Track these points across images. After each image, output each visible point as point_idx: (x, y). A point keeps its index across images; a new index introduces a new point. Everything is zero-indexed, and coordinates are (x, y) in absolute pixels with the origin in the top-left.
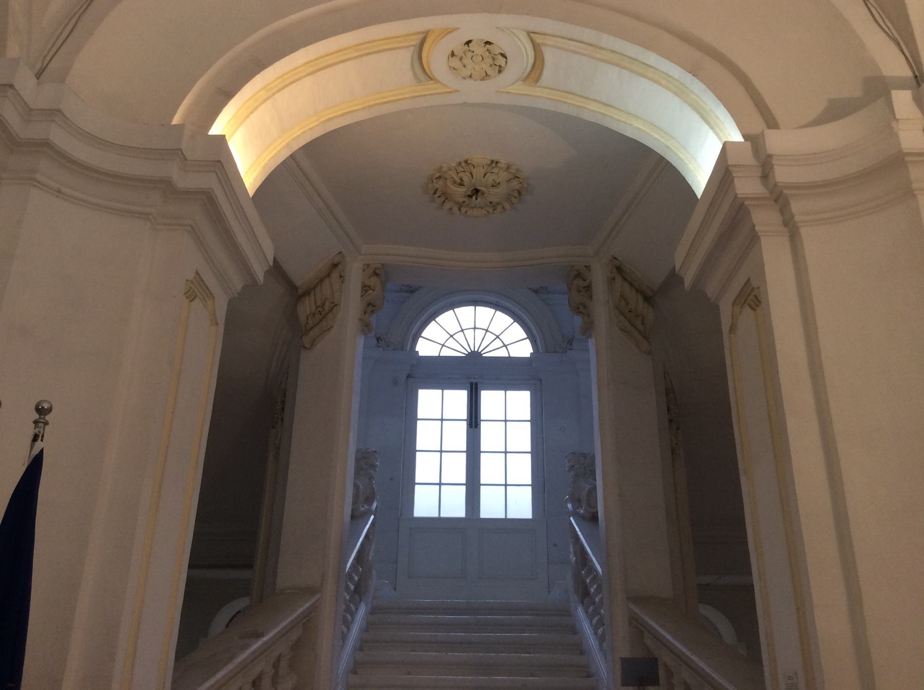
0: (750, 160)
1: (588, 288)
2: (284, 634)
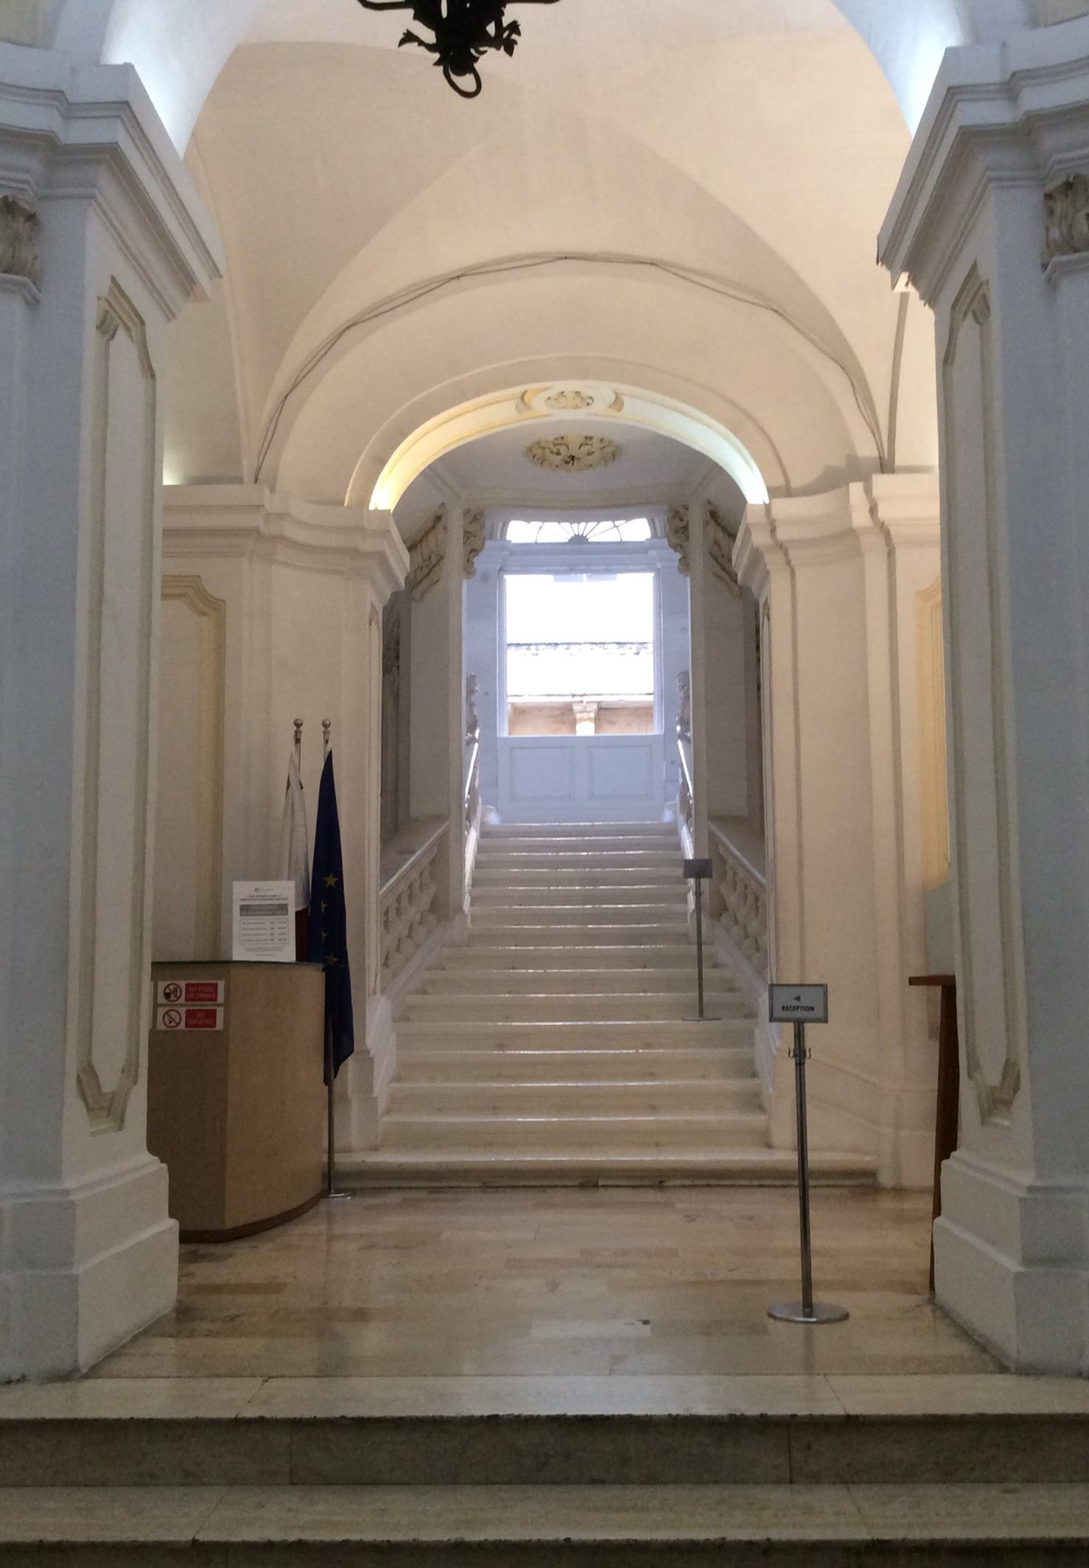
0: (763, 519)
1: (685, 528)
2: (425, 853)
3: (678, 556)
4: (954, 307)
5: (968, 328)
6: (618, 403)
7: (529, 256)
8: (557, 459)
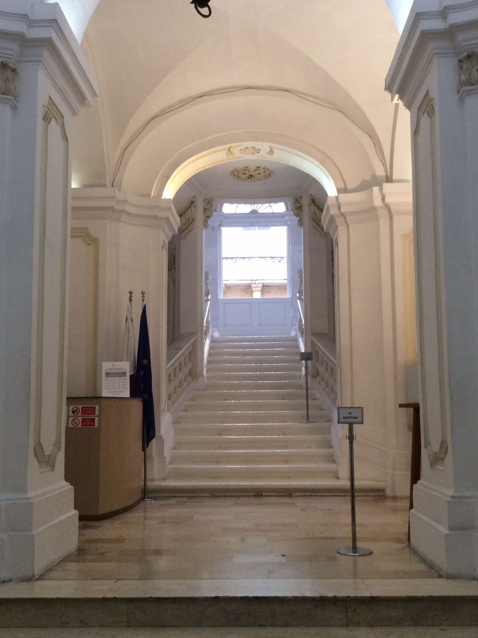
0: (335, 203)
1: (301, 207)
2: (187, 350)
3: (298, 219)
4: (419, 110)
5: (425, 119)
6: (271, 152)
7: (232, 87)
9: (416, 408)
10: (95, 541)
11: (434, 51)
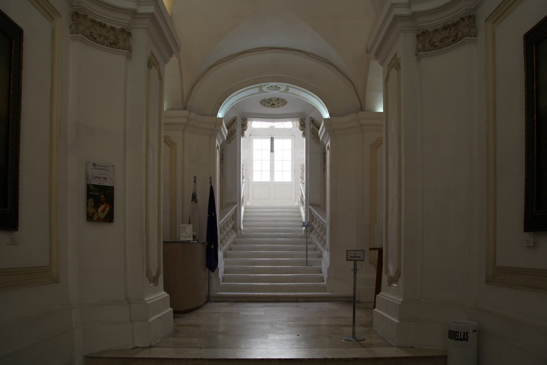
1: (304, 124)
3: (302, 132)
4: (389, 65)
5: (394, 72)
6: (287, 90)
7: (264, 48)
8: (269, 105)
9: (380, 251)
10: (182, 326)
11: (402, 28)
